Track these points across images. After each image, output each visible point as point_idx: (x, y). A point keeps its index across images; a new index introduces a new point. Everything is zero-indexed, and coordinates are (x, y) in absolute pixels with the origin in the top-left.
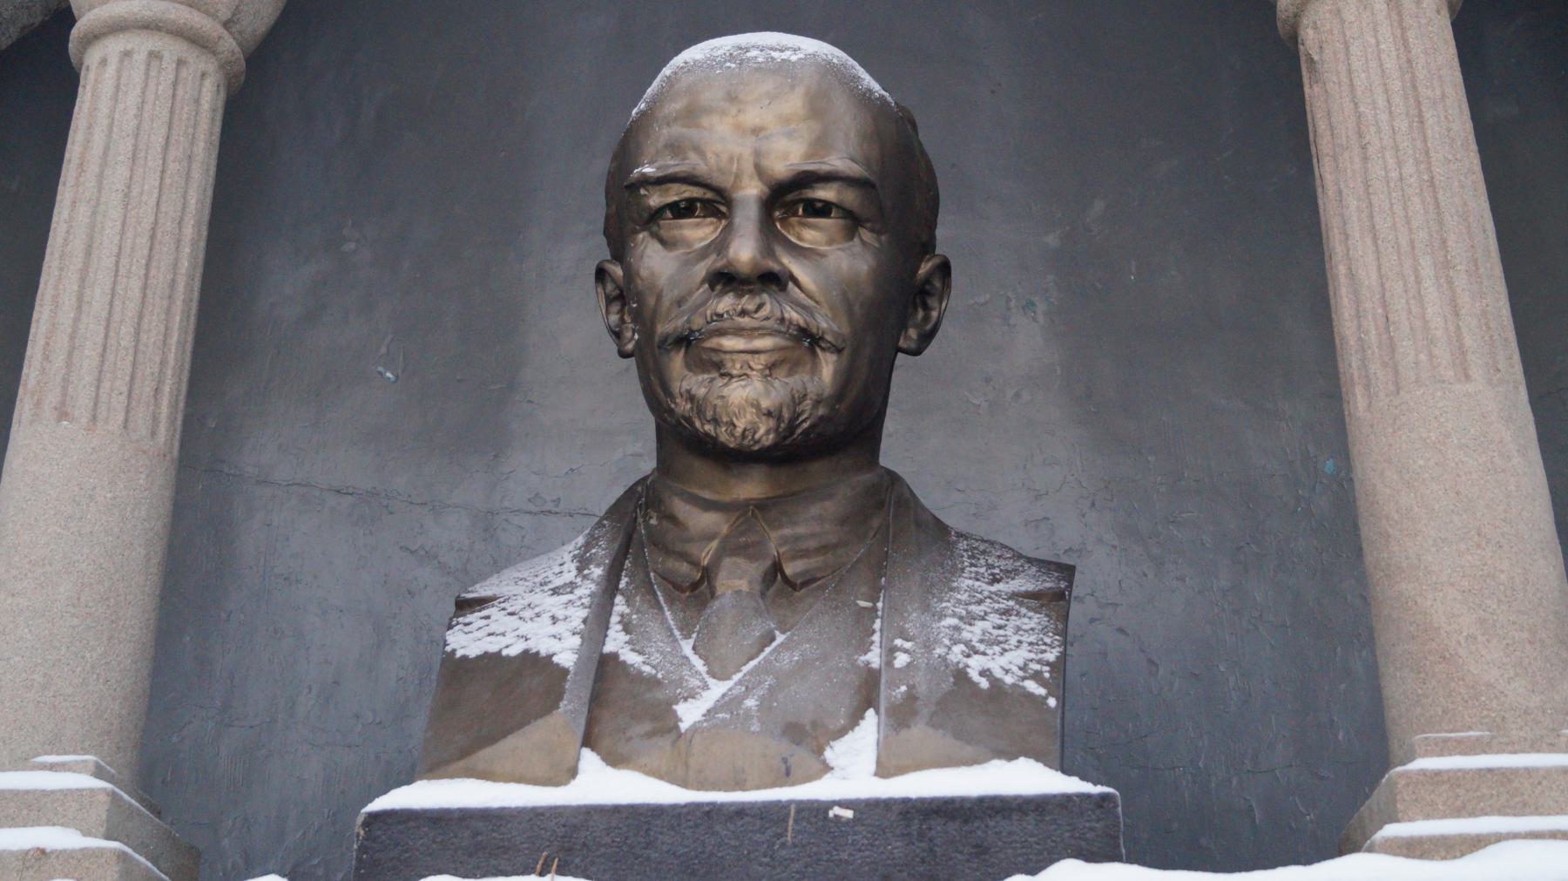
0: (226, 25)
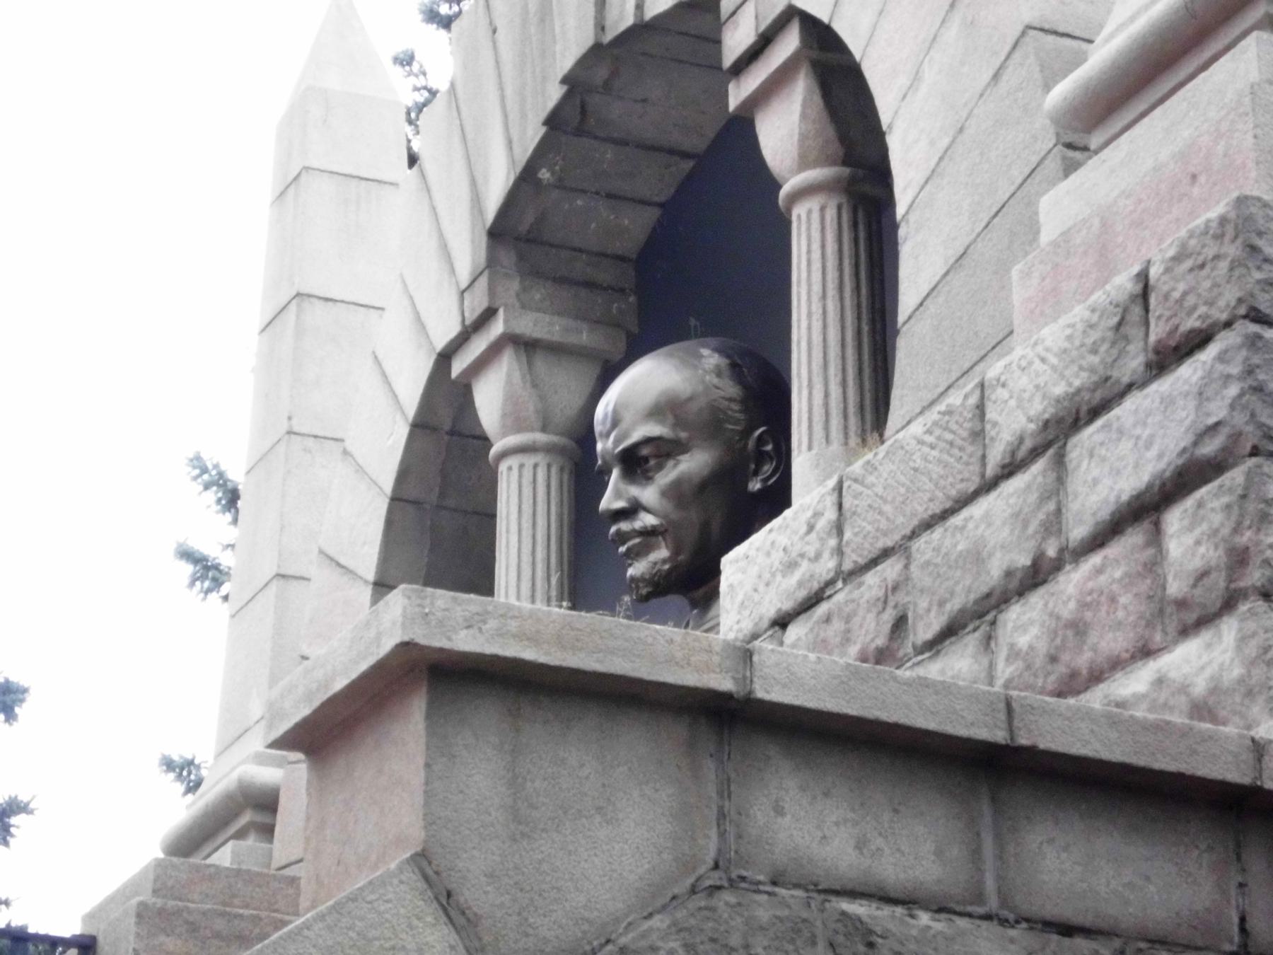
0: (544, 429)
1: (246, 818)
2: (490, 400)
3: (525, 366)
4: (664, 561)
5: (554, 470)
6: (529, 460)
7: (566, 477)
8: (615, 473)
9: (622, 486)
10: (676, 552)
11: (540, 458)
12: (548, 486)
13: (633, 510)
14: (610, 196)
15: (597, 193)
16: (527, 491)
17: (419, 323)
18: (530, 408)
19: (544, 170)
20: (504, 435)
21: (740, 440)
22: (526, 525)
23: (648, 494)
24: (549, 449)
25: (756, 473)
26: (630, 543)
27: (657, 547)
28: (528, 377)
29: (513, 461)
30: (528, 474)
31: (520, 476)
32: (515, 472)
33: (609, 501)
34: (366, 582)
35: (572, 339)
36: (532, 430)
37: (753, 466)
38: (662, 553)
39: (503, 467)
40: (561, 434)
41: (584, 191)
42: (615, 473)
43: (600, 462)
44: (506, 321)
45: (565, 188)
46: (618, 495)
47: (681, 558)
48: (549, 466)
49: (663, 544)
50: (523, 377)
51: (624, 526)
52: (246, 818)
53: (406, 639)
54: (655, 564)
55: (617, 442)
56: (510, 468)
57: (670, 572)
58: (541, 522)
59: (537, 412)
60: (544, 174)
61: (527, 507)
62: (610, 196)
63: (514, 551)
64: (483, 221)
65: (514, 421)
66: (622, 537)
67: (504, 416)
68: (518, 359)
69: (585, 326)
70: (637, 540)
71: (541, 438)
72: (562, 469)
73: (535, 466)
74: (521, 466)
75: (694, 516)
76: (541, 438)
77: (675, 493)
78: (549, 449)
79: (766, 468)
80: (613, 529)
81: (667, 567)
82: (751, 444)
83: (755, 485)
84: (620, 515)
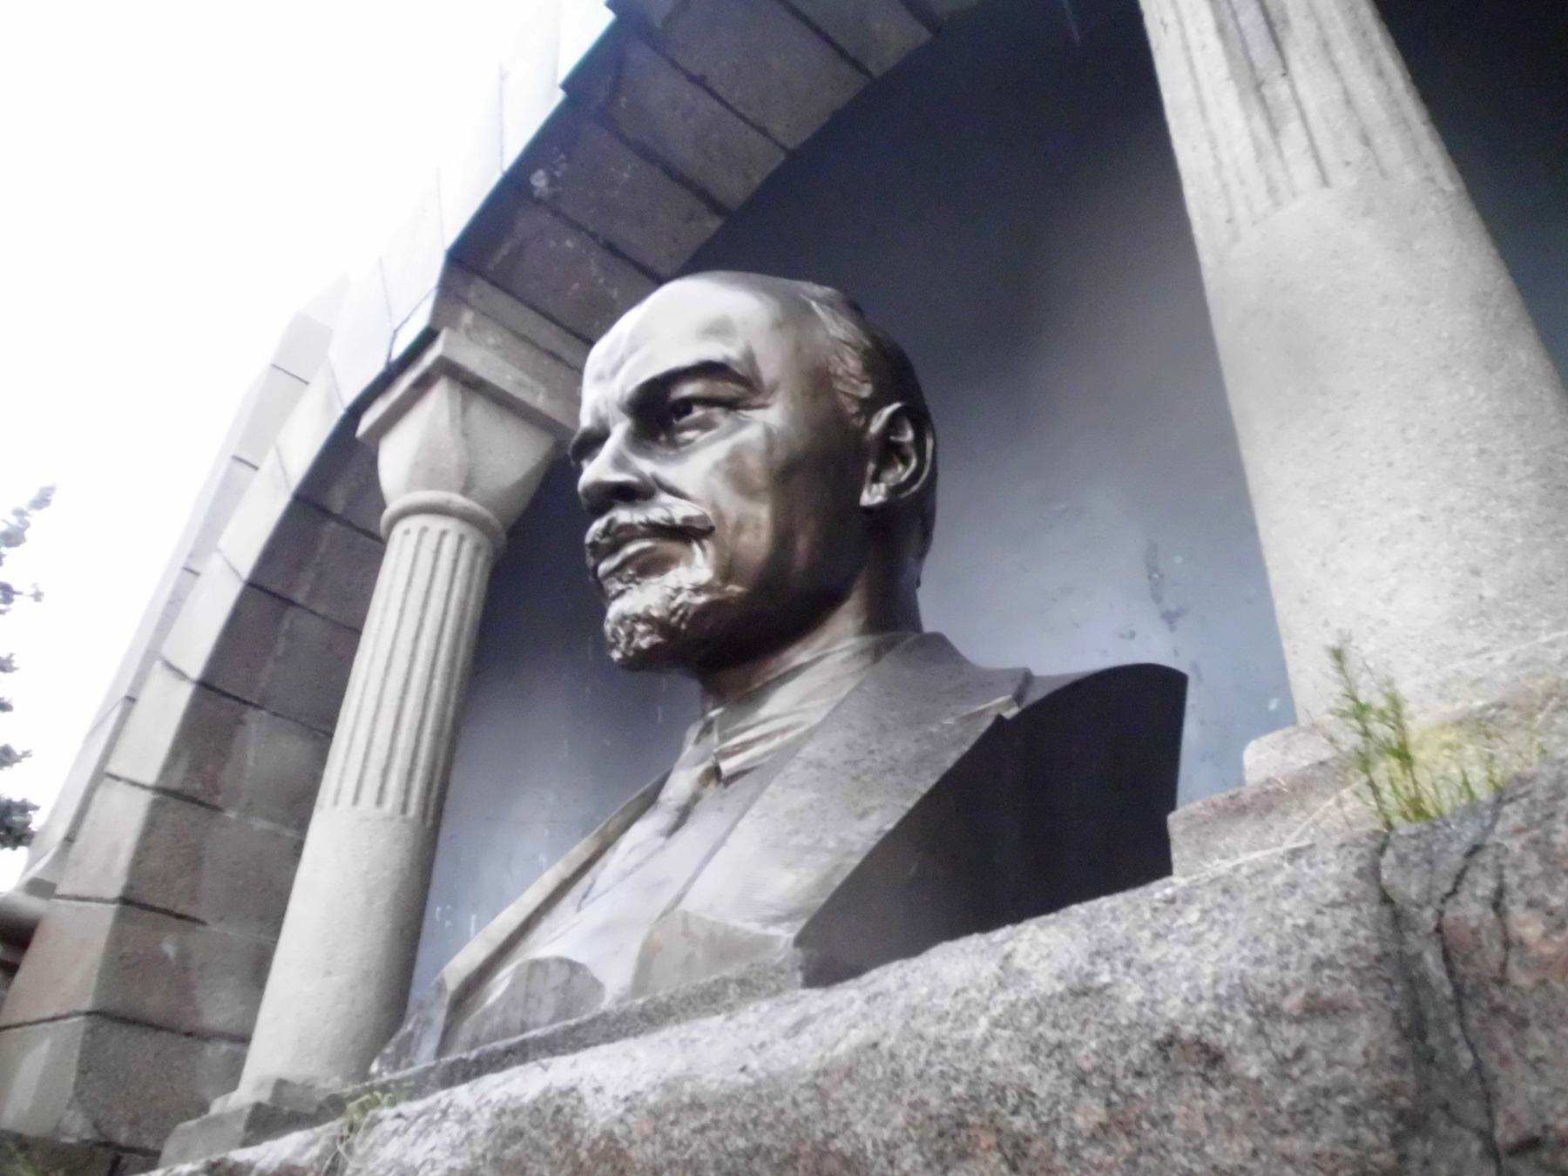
0: (466, 491)
2: (398, 463)
3: (458, 410)
5: (467, 546)
6: (436, 524)
7: (480, 560)
10: (727, 572)
12: (456, 562)
14: (611, 248)
15: (594, 236)
18: (453, 458)
19: (541, 173)
21: (858, 415)
24: (465, 517)
25: (876, 479)
26: (631, 549)
28: (458, 421)
29: (414, 523)
30: (430, 541)
31: (419, 542)
32: (414, 537)
33: (596, 470)
35: (523, 395)
36: (449, 489)
37: (871, 467)
40: (485, 505)
41: (579, 228)
44: (447, 343)
45: (557, 213)
46: (619, 463)
48: (462, 538)
50: (452, 420)
51: (623, 515)
53: (580, 958)
56: (407, 532)
57: (703, 611)
58: (436, 603)
60: (539, 181)
61: (420, 583)
62: (611, 248)
66: (618, 537)
68: (451, 398)
69: (542, 389)
70: (647, 544)
71: (459, 500)
72: (477, 548)
73: (444, 533)
74: (424, 530)
78: (465, 517)
81: (701, 599)
82: (876, 425)
83: (873, 496)
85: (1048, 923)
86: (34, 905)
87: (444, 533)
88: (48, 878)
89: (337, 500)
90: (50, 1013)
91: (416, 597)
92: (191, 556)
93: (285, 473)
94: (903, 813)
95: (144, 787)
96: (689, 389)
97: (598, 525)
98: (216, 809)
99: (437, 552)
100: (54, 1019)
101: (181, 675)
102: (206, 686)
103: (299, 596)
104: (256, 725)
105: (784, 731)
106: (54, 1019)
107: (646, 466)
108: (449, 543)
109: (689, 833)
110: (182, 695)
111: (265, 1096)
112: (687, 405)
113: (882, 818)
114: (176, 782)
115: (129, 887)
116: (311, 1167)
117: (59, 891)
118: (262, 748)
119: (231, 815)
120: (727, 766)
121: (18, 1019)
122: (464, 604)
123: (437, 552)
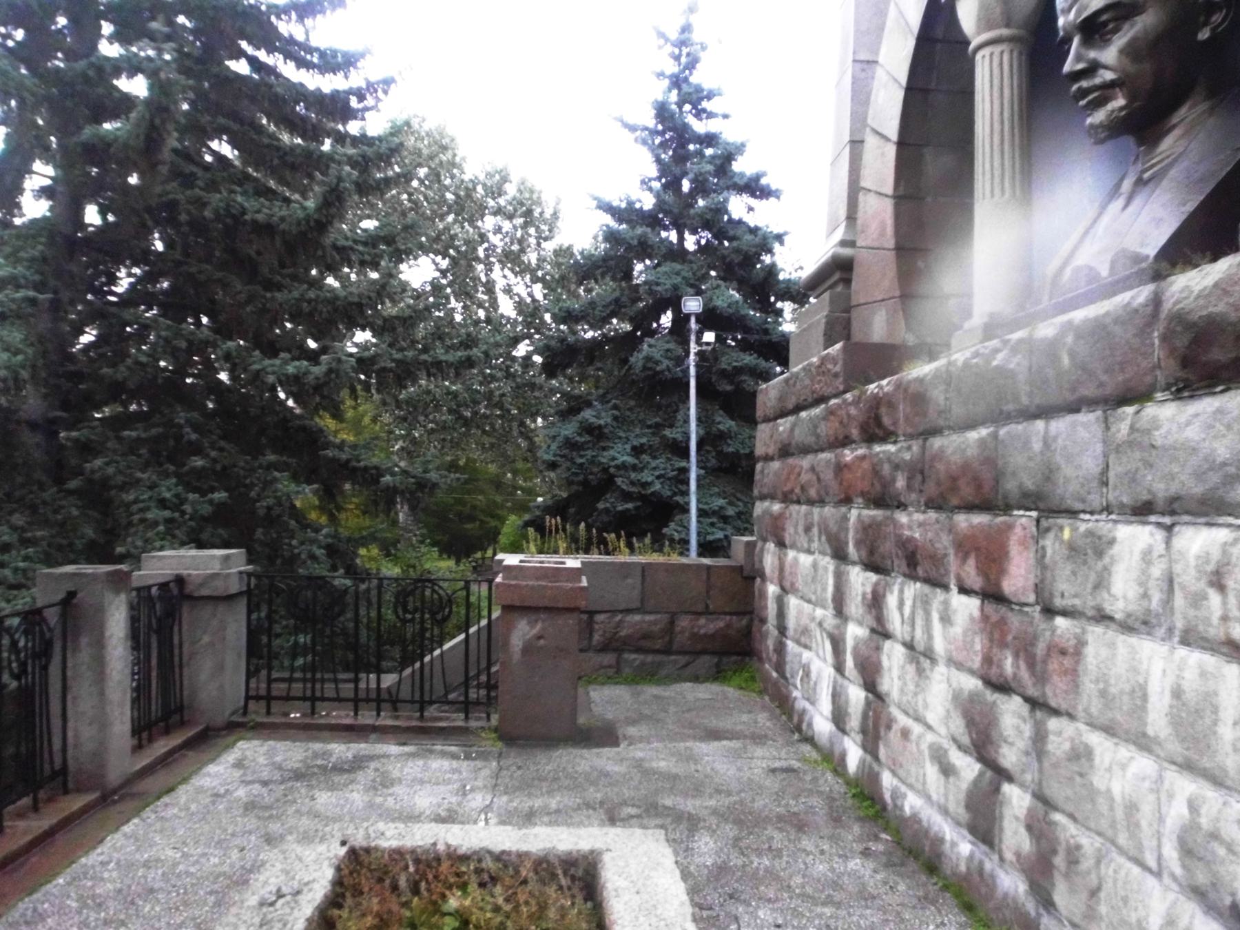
0: (1007, 26)
1: (837, 276)
4: (1121, 109)
5: (1015, 54)
6: (997, 49)
7: (1024, 58)
8: (1076, 41)
9: (1083, 51)
10: (1131, 98)
11: (1004, 47)
13: (1093, 68)
16: (996, 71)
17: (896, 80)
20: (979, 33)
22: (996, 94)
23: (1109, 55)
24: (1010, 39)
25: (1205, 24)
26: (1091, 97)
27: (1114, 98)
29: (986, 52)
32: (987, 58)
34: (887, 196)
38: (1120, 102)
39: (978, 57)
42: (1076, 41)
43: (1061, 33)
46: (1079, 58)
47: (1136, 104)
48: (1011, 51)
49: (1120, 94)
51: (1085, 84)
52: (837, 276)
54: (1113, 111)
55: (1079, 13)
59: (1002, 13)
61: (996, 82)
63: (988, 113)
64: (911, 31)
65: (986, 22)
67: (979, 20)
71: (1005, 32)
72: (1020, 54)
73: (1002, 53)
74: (992, 54)
75: (1147, 67)
76: (1005, 32)
77: (1130, 51)
79: (1214, 19)
80: (1075, 87)
81: (1123, 113)
83: (1204, 35)
84: (1077, 76)
85: (239, 655)
86: (847, 252)
87: (1002, 53)
88: (848, 238)
89: (939, 32)
90: (880, 298)
91: (992, 80)
92: (854, 53)
93: (907, 23)
94: (1184, 217)
95: (887, 196)
96: (1104, 17)
97: (1075, 87)
98: (923, 199)
99: (1001, 64)
100: (883, 300)
101: (887, 139)
102: (902, 144)
103: (933, 86)
104: (928, 153)
105: (1168, 157)
106: (883, 300)
107: (1092, 54)
108: (1006, 57)
109: (1131, 209)
110: (891, 151)
111: (986, 319)
112: (1105, 24)
113: (1190, 207)
114: (901, 192)
115: (897, 243)
116: (869, 418)
117: (858, 244)
118: (935, 164)
119: (929, 199)
120: (1146, 175)
121: (862, 301)
122: (1020, 86)
123: (1001, 64)
